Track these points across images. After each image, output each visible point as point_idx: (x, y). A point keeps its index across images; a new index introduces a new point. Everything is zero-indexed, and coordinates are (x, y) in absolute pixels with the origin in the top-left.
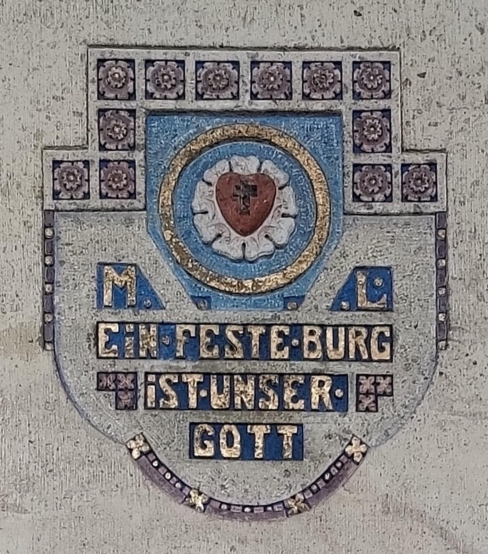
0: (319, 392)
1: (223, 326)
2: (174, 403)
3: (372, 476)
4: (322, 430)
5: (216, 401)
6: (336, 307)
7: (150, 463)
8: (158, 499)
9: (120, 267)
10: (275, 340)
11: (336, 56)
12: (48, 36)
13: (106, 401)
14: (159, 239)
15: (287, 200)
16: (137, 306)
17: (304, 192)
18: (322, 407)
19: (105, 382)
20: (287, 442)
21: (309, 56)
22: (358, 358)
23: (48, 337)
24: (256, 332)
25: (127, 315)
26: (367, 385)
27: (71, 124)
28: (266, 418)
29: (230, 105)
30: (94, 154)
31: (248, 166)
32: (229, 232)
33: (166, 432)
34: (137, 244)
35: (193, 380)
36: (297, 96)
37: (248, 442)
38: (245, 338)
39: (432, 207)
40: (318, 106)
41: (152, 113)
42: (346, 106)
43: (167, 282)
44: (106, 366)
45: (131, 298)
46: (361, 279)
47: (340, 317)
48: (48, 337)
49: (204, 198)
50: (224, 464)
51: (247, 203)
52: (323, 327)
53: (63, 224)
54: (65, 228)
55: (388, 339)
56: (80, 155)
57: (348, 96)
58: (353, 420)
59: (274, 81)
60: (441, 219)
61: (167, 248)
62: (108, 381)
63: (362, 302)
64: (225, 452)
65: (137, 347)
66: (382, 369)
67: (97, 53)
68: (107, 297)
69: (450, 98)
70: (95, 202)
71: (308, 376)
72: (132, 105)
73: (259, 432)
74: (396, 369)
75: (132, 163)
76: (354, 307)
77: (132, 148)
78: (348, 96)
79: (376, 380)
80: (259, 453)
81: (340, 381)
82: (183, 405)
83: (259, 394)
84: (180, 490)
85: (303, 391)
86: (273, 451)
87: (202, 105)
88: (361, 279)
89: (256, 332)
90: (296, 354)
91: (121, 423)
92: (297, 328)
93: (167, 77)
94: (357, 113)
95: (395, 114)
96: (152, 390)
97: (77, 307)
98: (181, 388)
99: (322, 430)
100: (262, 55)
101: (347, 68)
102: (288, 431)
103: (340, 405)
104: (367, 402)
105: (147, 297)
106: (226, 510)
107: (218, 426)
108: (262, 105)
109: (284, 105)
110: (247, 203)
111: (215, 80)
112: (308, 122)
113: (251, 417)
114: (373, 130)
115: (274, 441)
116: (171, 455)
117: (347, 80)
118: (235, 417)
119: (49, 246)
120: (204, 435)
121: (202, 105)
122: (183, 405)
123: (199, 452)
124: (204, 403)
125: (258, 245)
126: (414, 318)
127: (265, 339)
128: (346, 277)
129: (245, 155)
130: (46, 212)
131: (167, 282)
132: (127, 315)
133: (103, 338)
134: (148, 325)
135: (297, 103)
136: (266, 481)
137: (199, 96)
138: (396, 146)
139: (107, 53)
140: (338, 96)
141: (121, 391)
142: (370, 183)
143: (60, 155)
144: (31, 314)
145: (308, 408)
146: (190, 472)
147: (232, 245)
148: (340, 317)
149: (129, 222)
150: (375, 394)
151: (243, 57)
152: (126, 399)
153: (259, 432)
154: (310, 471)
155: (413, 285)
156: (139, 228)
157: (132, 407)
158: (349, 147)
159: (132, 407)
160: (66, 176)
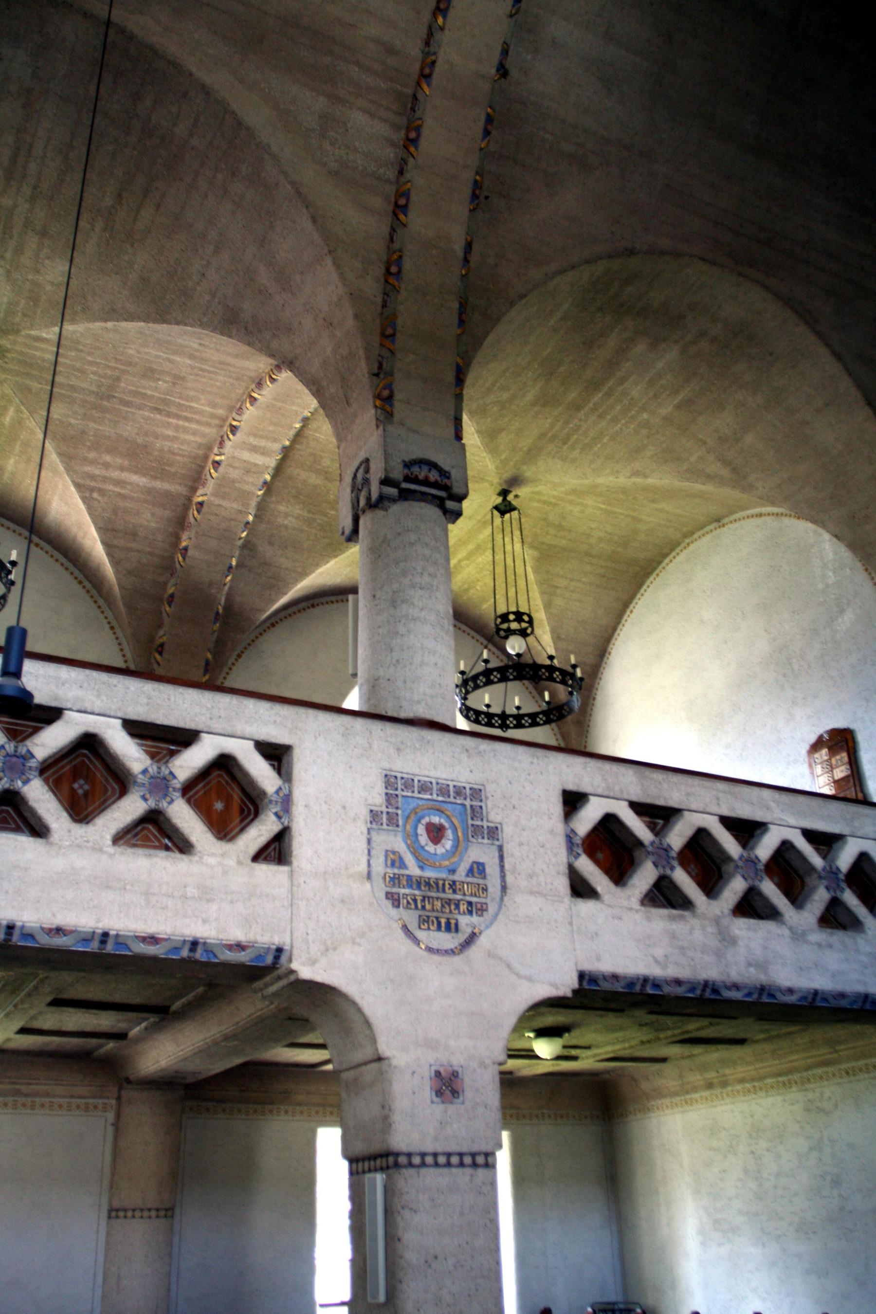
0: (463, 907)
1: (429, 879)
2: (413, 906)
3: (483, 941)
4: (464, 921)
5: (428, 907)
6: (467, 875)
7: (405, 928)
8: (408, 944)
9: (394, 853)
10: (447, 886)
11: (464, 785)
12: (369, 764)
13: (389, 903)
14: (406, 843)
15: (449, 833)
16: (400, 867)
17: (455, 830)
18: (464, 913)
19: (389, 896)
20: (453, 926)
21: (455, 783)
22: (475, 895)
23: (369, 876)
24: (441, 883)
25: (396, 871)
26: (479, 906)
27: (377, 799)
28: (445, 916)
29: (429, 797)
30: (384, 809)
31: (436, 820)
32: (430, 844)
33: (411, 917)
34: (399, 844)
35: (419, 898)
36: (452, 797)
37: (439, 924)
38: (437, 884)
39: (497, 843)
40: (459, 801)
41: (403, 796)
42: (468, 803)
43: (409, 860)
44: (389, 889)
45: (397, 864)
46: (475, 866)
47: (470, 880)
48: (369, 876)
49: (421, 830)
50: (431, 932)
51: (436, 833)
52: (463, 883)
53: (373, 833)
54: (375, 836)
55: (485, 890)
56: (379, 809)
57: (468, 800)
58: (475, 919)
59: (444, 790)
60: (500, 848)
61: (408, 847)
62: (389, 896)
63: (476, 874)
64: (431, 927)
65: (399, 883)
66: (483, 900)
67: (385, 772)
68: (389, 863)
69: (502, 805)
70: (385, 826)
71: (459, 901)
72: (397, 793)
73: (443, 921)
74: (488, 901)
75: (397, 814)
76: (473, 876)
77: (397, 808)
78: (468, 800)
79: (482, 904)
80: (443, 929)
81: (470, 904)
82: (416, 907)
83: (443, 906)
84: (417, 941)
85: (457, 906)
86: (448, 928)
87: (420, 796)
88: (475, 866)
89: (441, 883)
90: (454, 892)
91: (394, 912)
92: (454, 882)
93: (408, 784)
94: (471, 806)
95: (484, 808)
96: (405, 901)
97: (379, 866)
98: (415, 901)
99: (464, 921)
100: (440, 781)
101: (468, 789)
102: (453, 922)
103: (470, 913)
104: (480, 913)
105: (403, 865)
106: (437, 952)
107: (428, 917)
108: (440, 798)
109: (448, 800)
110: (436, 833)
111: (424, 788)
112: (455, 806)
113: (439, 915)
114: (476, 812)
115: (448, 924)
116: (413, 926)
117: (468, 794)
118: (435, 914)
119: (369, 841)
120: (424, 920)
121: (420, 796)
122: (416, 907)
123: (422, 927)
124: (423, 907)
125: (440, 850)
126: (493, 882)
127: (444, 885)
128: (151, 325)
129: (435, 815)
130: (369, 829)
131: (409, 860)
132: (396, 871)
133: (388, 879)
134: (403, 875)
135: (452, 799)
136: (446, 940)
137: (419, 792)
138: (485, 819)
139: (389, 773)
140: (465, 799)
141: (395, 900)
142: (477, 831)
143: (373, 808)
144: (363, 867)
145: (459, 913)
146: (421, 935)
147: (431, 848)
148: (470, 880)
149: (396, 836)
150: (482, 910)
151: (434, 781)
152: (396, 903)
153: (443, 921)
154: (461, 937)
155: (492, 870)
156: (399, 838)
157: (398, 906)
158: (469, 818)
159: (398, 906)
160: (374, 816)
